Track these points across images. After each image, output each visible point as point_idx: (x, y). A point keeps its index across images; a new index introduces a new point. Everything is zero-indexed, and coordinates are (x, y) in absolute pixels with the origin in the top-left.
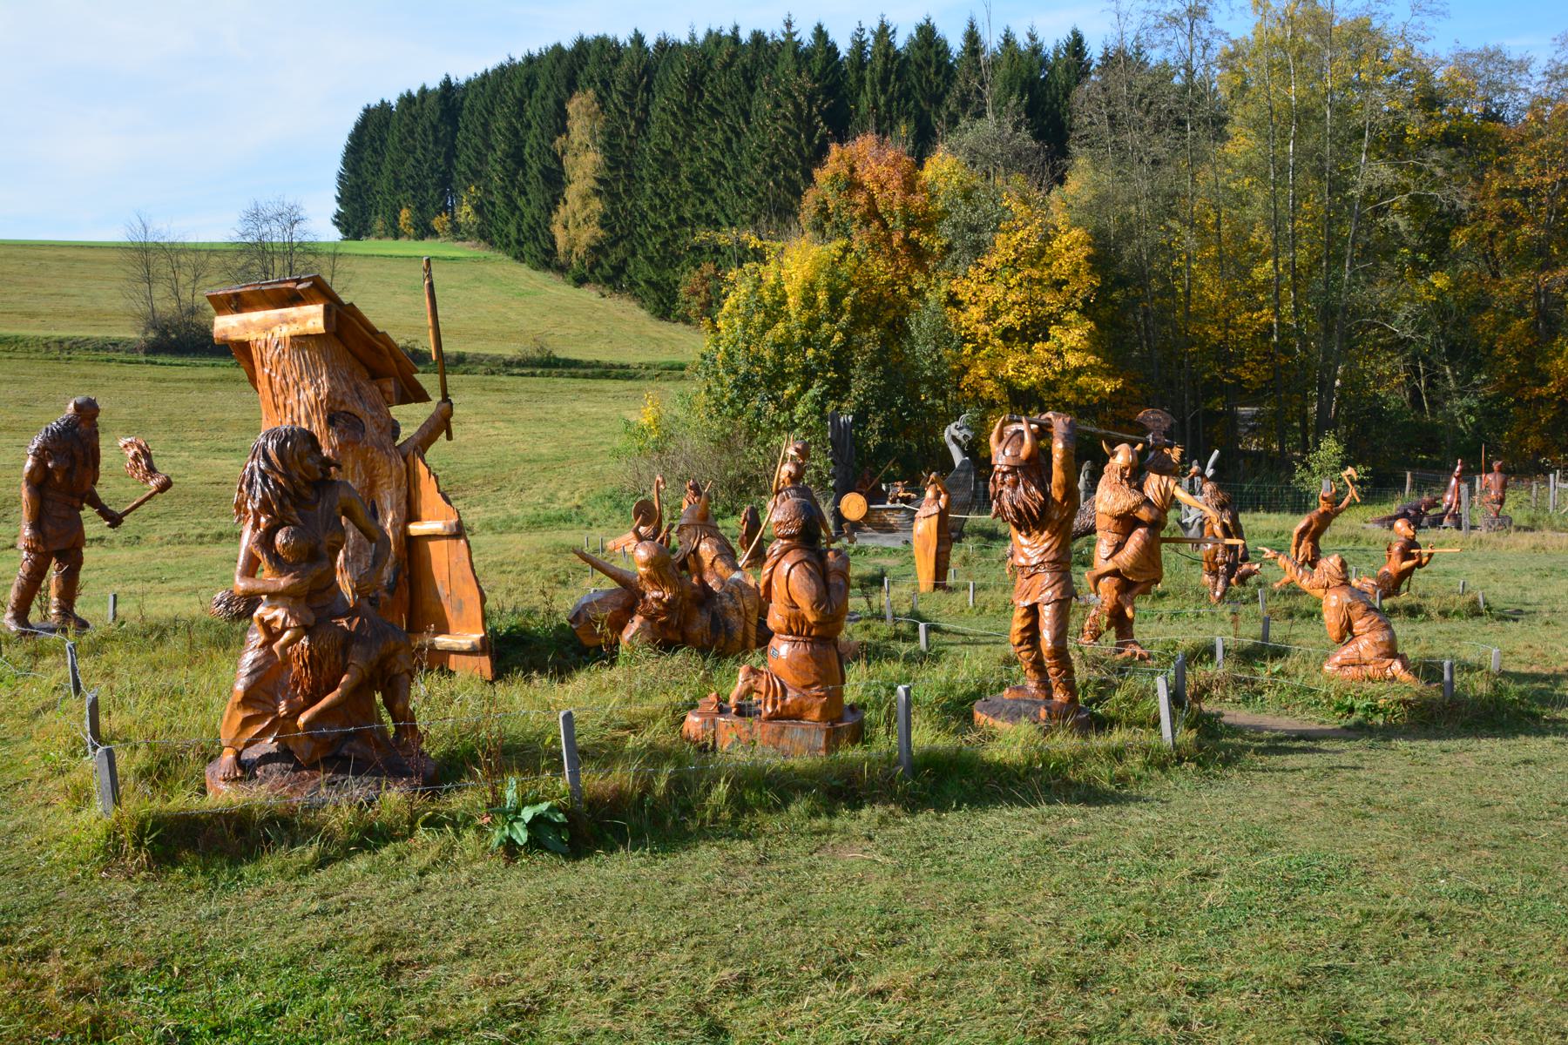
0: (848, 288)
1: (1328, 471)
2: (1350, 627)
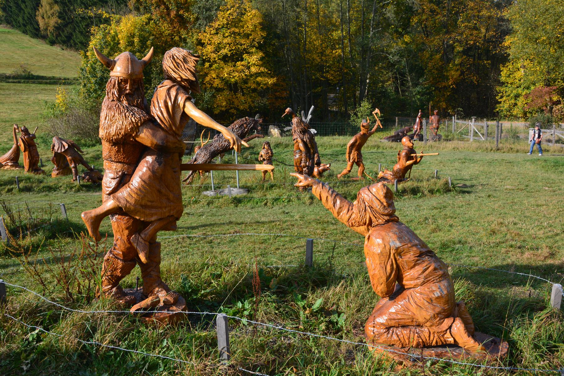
0: (149, 36)
1: (366, 115)
2: (399, 277)
